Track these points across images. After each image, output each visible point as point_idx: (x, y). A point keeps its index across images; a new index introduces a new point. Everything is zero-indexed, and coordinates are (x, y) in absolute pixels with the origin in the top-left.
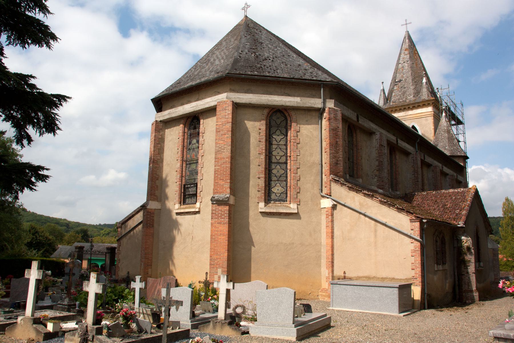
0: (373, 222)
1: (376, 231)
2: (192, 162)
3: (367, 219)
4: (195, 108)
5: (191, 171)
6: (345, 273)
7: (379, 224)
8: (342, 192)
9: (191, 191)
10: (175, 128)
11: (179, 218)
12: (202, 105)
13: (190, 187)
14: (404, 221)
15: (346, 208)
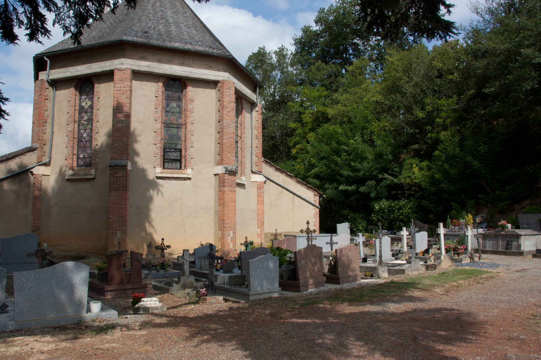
0: (292, 195)
1: (293, 201)
2: (171, 126)
3: (288, 192)
4: (188, 73)
5: (170, 135)
6: (276, 230)
7: (295, 196)
8: (269, 171)
9: (174, 155)
10: (149, 84)
11: (160, 181)
12: (196, 73)
13: (169, 152)
14: (311, 195)
15: (273, 184)
